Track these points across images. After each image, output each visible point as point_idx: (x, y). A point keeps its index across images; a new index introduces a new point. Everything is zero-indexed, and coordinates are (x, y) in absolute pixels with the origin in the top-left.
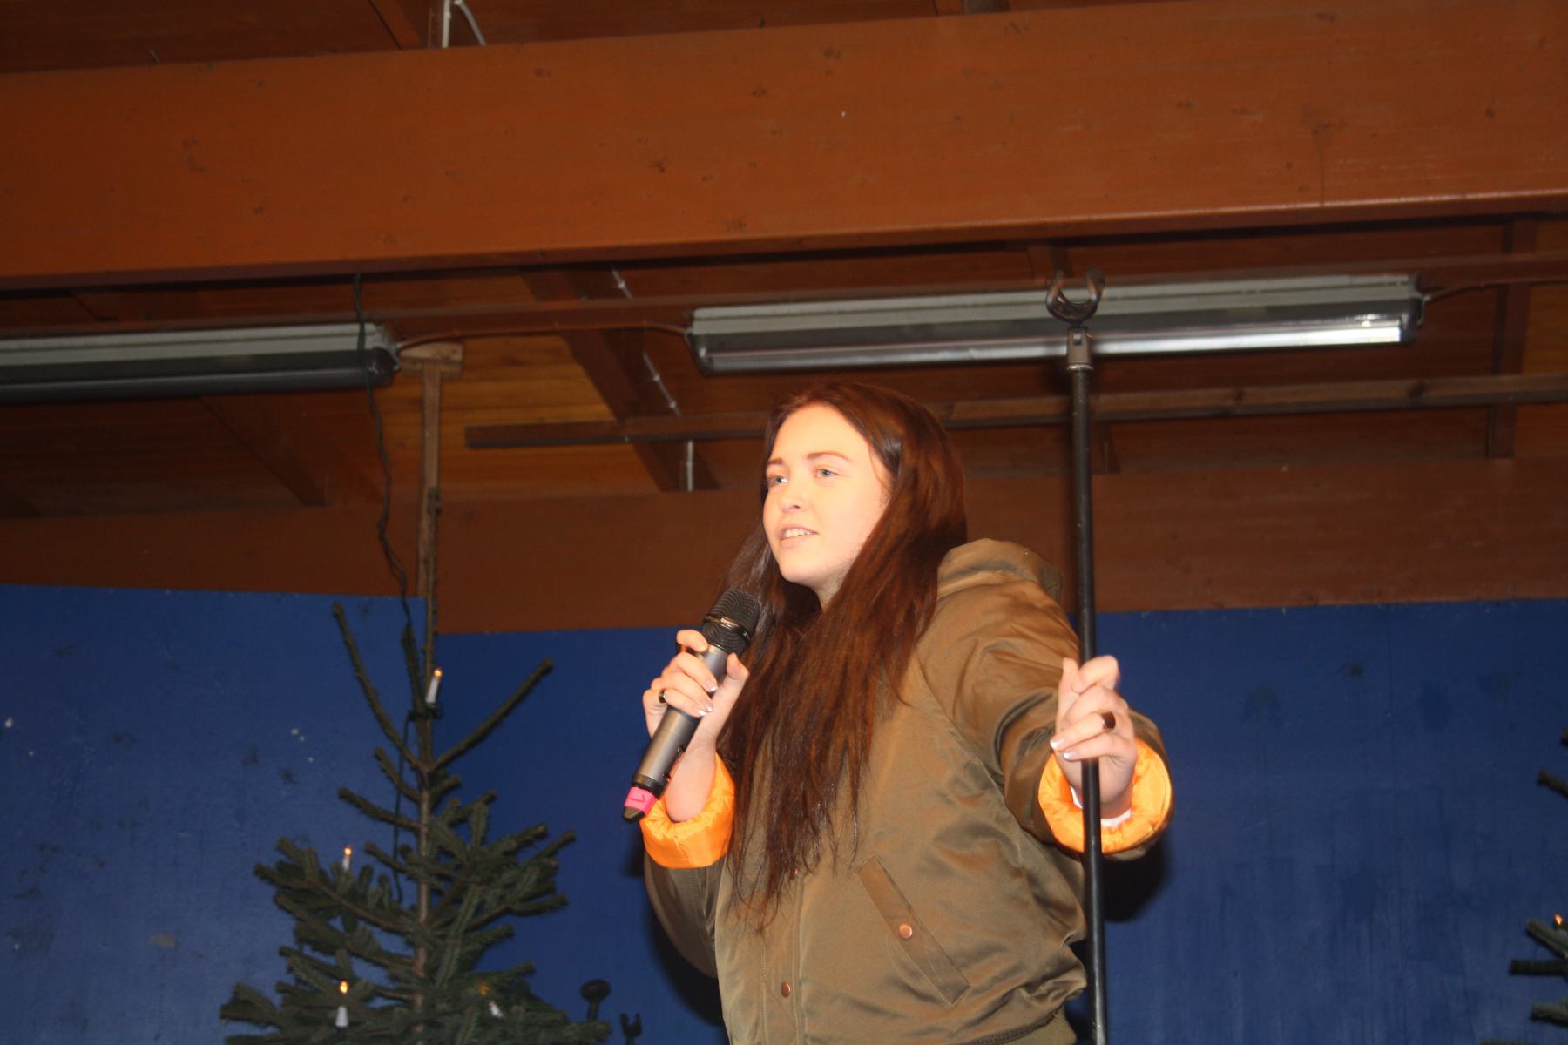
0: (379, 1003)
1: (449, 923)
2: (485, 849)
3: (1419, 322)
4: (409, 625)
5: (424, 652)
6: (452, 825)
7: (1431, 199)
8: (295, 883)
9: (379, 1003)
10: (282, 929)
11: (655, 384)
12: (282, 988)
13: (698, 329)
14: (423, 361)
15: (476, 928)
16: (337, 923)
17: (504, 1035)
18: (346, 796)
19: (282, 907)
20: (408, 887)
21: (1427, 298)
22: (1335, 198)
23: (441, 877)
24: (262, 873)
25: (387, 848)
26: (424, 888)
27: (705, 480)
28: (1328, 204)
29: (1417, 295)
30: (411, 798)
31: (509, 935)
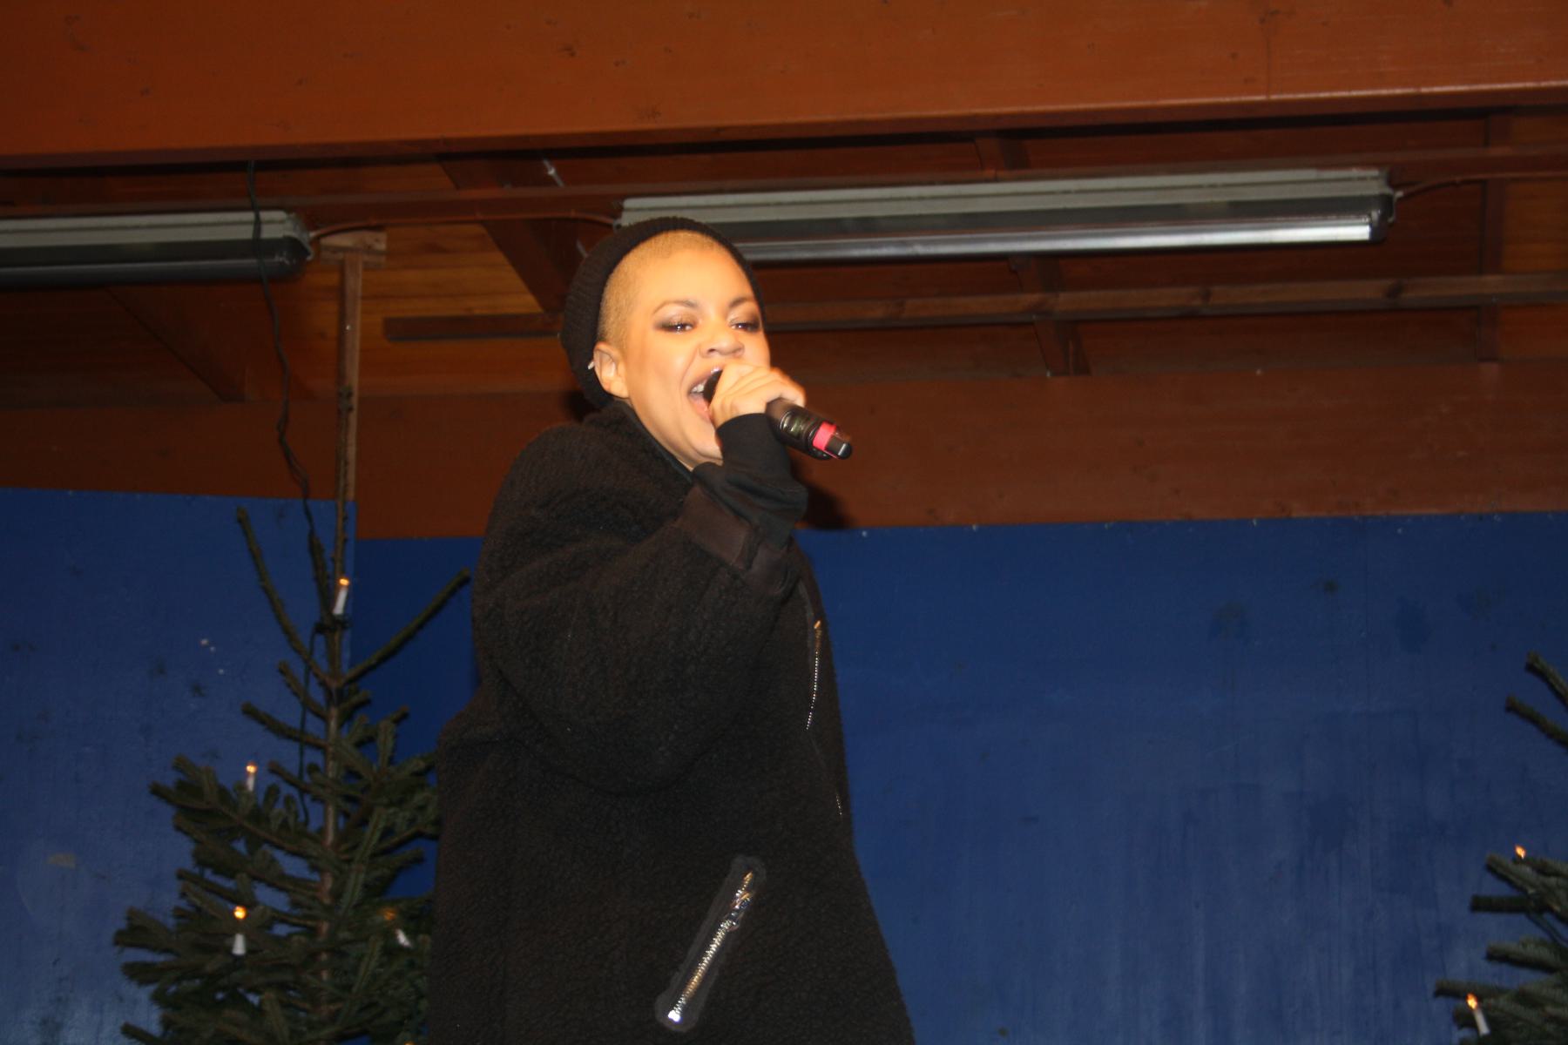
0: (281, 930)
1: (355, 847)
2: (392, 769)
3: (1391, 220)
4: (312, 533)
5: (333, 560)
6: (359, 744)
7: (1384, 92)
8: (198, 805)
9: (281, 930)
10: (180, 851)
12: (180, 914)
14: (344, 249)
15: (386, 852)
16: (240, 846)
17: (412, 965)
18: (250, 712)
19: (178, 828)
20: (315, 810)
21: (1399, 194)
22: (1282, 92)
23: (349, 799)
24: (157, 791)
25: (292, 767)
26: (331, 809)
28: (1274, 97)
29: (1388, 191)
30: (318, 715)
31: (419, 860)
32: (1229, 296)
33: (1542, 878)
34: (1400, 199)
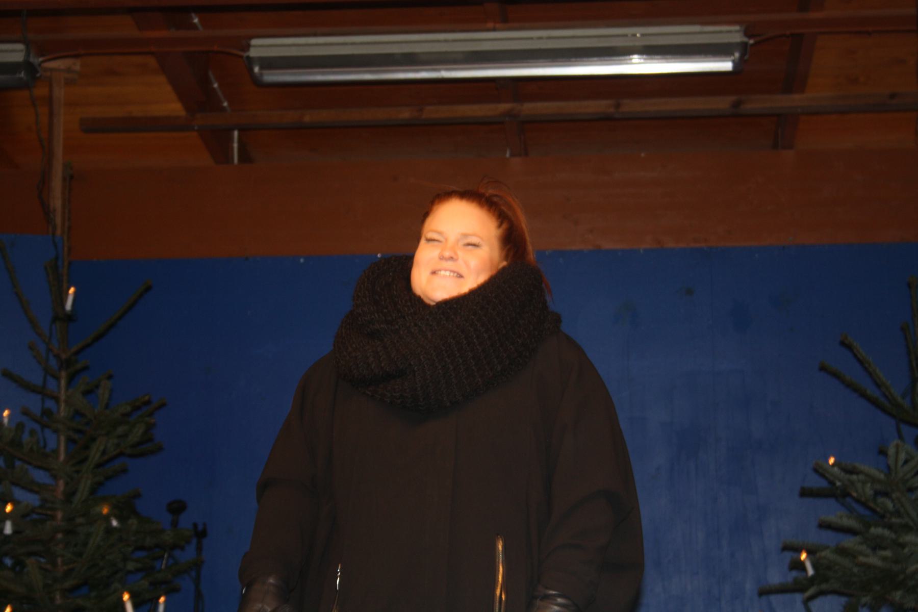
4: (57, 258)
9: (35, 516)
11: (214, 89)
13: (253, 53)
21: (752, 42)
25: (36, 410)
26: (62, 438)
27: (245, 157)
29: (745, 39)
31: (124, 471)
32: (434, 112)
33: (848, 476)
34: (752, 45)
